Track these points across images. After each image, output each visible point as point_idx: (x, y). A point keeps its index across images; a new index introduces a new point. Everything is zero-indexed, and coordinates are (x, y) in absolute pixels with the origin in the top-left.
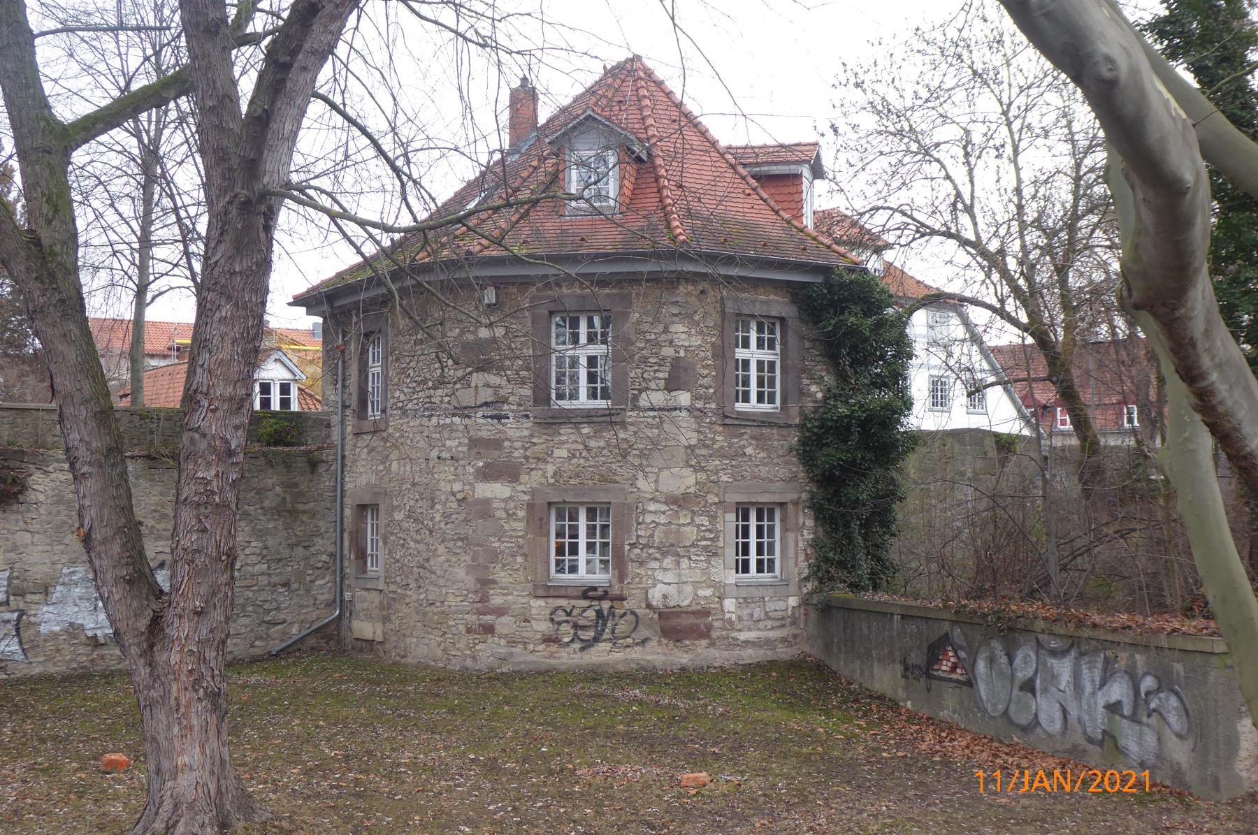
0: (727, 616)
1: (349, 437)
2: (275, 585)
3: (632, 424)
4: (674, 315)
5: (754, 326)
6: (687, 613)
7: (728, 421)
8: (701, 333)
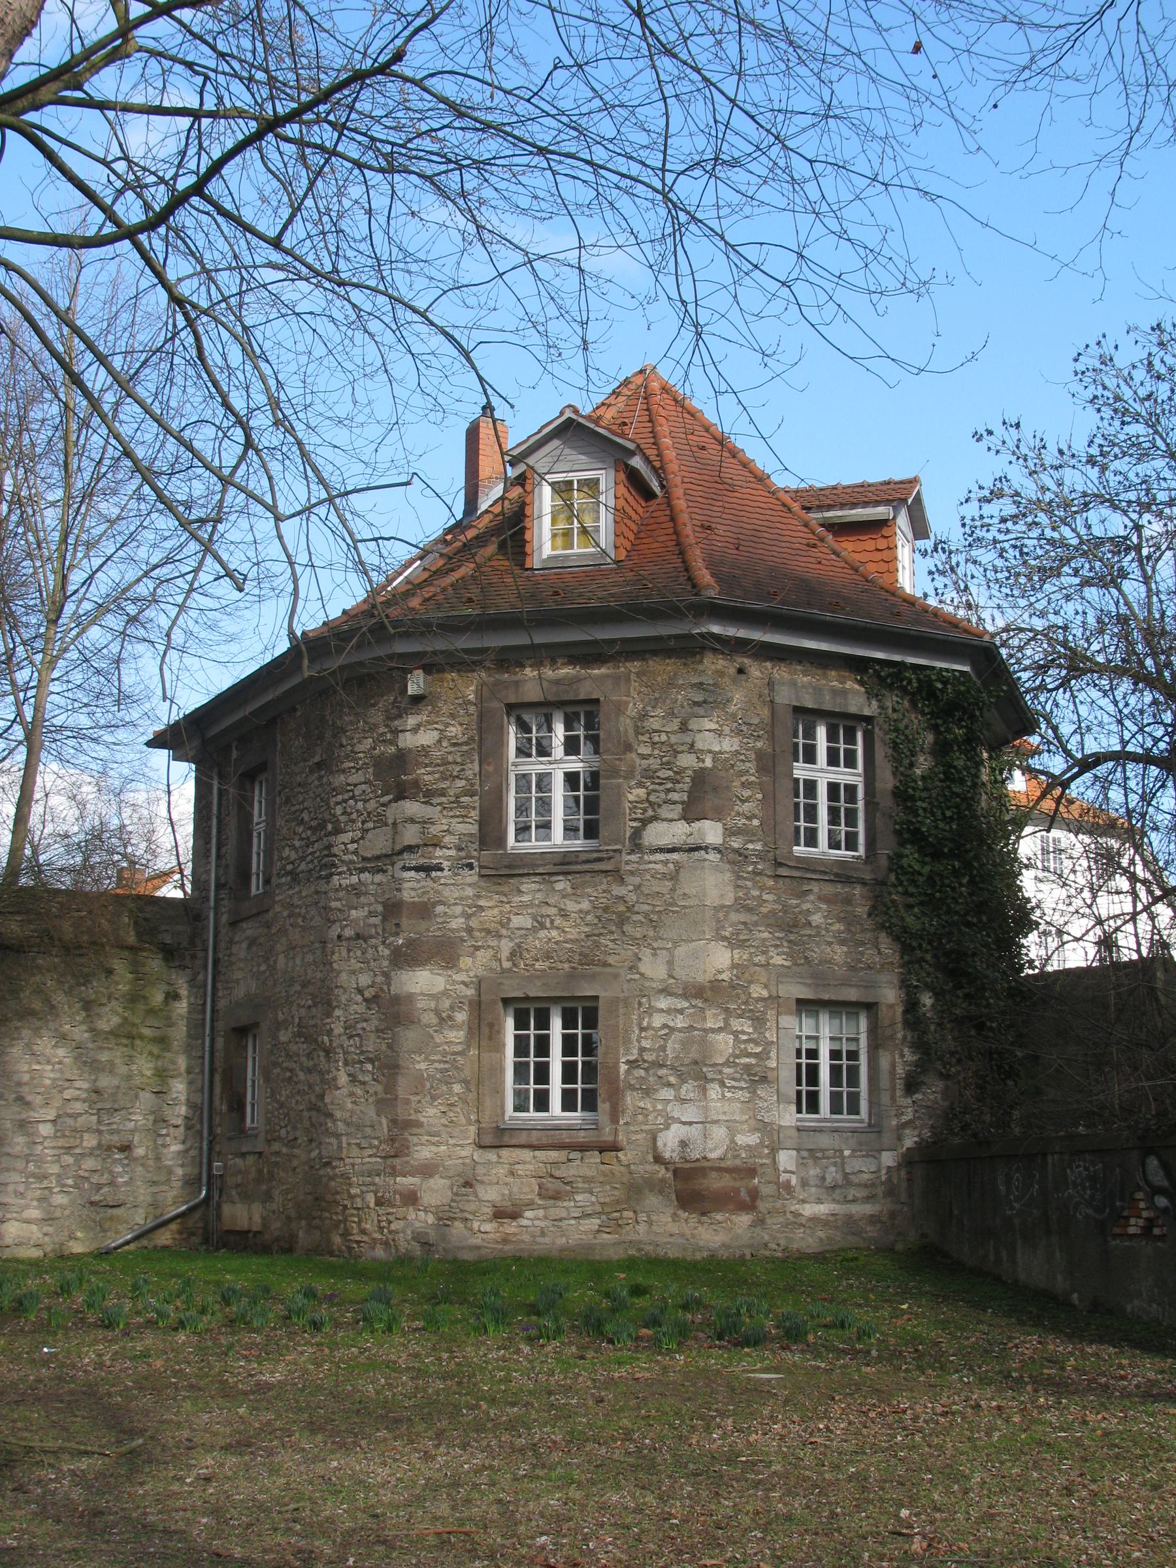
0: (783, 1177)
1: (223, 931)
2: (109, 1148)
3: (632, 873)
4: (696, 704)
5: (821, 732)
6: (719, 1169)
7: (783, 872)
8: (739, 732)
